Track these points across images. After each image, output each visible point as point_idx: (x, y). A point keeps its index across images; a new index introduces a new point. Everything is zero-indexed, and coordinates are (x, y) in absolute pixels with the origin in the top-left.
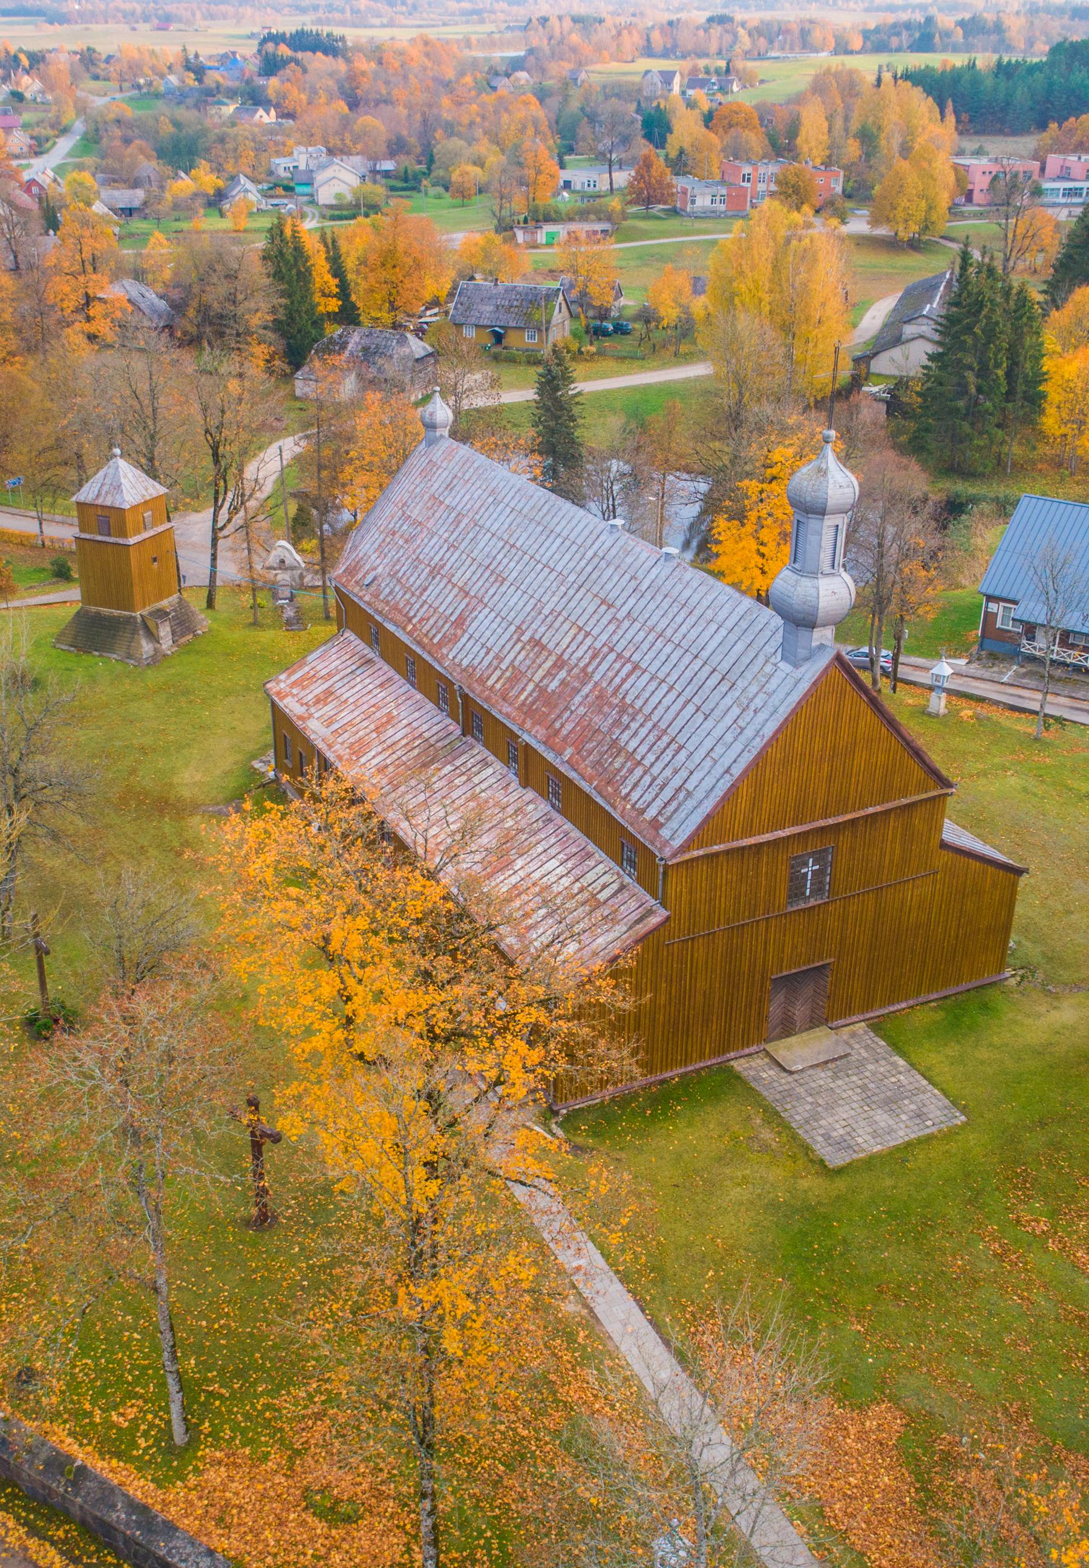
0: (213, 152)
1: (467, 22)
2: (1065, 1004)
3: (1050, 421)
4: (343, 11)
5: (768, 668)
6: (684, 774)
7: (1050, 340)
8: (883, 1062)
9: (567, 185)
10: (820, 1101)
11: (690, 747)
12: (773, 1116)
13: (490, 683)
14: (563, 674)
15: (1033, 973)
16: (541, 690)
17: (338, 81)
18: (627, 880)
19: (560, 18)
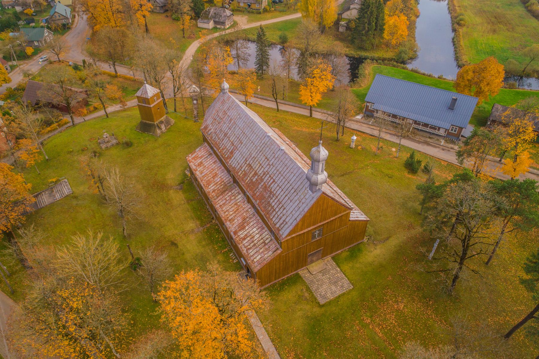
2: (378, 247)
3: (386, 35)
5: (306, 191)
6: (285, 216)
7: (386, 11)
11: (287, 209)
12: (308, 289)
13: (239, 174)
14: (256, 177)
18: (273, 238)
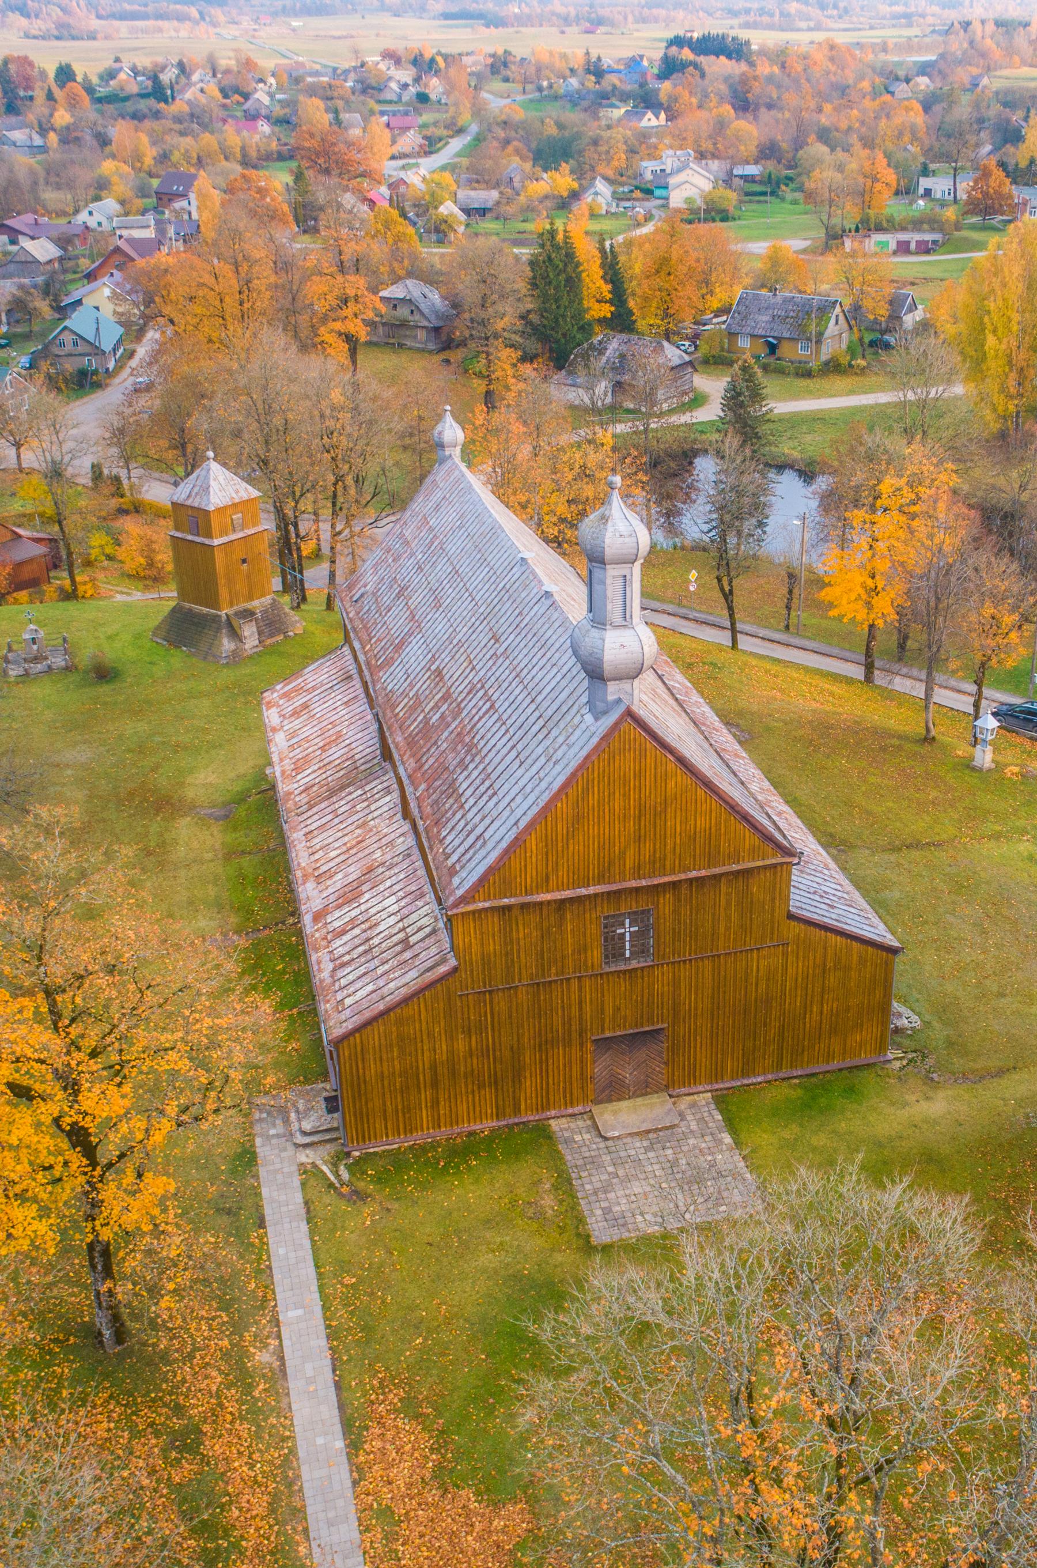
0: (586, 154)
1: (894, 26)
2: (941, 1094)
4: (772, 15)
8: (708, 1138)
9: (928, 192)
10: (621, 1173)
11: (501, 794)
12: (564, 1184)
15: (924, 1056)
16: (426, 720)
17: (731, 86)
19: (983, 22)
